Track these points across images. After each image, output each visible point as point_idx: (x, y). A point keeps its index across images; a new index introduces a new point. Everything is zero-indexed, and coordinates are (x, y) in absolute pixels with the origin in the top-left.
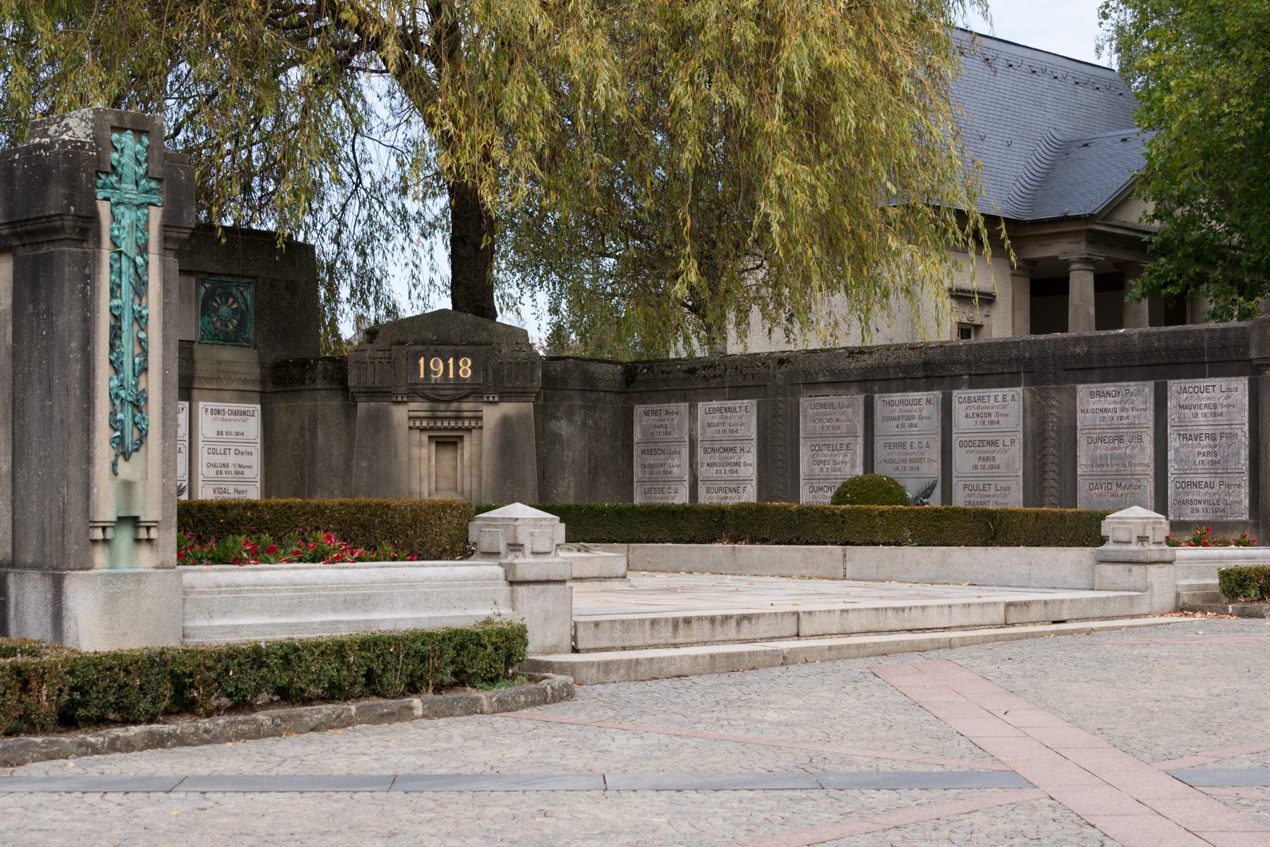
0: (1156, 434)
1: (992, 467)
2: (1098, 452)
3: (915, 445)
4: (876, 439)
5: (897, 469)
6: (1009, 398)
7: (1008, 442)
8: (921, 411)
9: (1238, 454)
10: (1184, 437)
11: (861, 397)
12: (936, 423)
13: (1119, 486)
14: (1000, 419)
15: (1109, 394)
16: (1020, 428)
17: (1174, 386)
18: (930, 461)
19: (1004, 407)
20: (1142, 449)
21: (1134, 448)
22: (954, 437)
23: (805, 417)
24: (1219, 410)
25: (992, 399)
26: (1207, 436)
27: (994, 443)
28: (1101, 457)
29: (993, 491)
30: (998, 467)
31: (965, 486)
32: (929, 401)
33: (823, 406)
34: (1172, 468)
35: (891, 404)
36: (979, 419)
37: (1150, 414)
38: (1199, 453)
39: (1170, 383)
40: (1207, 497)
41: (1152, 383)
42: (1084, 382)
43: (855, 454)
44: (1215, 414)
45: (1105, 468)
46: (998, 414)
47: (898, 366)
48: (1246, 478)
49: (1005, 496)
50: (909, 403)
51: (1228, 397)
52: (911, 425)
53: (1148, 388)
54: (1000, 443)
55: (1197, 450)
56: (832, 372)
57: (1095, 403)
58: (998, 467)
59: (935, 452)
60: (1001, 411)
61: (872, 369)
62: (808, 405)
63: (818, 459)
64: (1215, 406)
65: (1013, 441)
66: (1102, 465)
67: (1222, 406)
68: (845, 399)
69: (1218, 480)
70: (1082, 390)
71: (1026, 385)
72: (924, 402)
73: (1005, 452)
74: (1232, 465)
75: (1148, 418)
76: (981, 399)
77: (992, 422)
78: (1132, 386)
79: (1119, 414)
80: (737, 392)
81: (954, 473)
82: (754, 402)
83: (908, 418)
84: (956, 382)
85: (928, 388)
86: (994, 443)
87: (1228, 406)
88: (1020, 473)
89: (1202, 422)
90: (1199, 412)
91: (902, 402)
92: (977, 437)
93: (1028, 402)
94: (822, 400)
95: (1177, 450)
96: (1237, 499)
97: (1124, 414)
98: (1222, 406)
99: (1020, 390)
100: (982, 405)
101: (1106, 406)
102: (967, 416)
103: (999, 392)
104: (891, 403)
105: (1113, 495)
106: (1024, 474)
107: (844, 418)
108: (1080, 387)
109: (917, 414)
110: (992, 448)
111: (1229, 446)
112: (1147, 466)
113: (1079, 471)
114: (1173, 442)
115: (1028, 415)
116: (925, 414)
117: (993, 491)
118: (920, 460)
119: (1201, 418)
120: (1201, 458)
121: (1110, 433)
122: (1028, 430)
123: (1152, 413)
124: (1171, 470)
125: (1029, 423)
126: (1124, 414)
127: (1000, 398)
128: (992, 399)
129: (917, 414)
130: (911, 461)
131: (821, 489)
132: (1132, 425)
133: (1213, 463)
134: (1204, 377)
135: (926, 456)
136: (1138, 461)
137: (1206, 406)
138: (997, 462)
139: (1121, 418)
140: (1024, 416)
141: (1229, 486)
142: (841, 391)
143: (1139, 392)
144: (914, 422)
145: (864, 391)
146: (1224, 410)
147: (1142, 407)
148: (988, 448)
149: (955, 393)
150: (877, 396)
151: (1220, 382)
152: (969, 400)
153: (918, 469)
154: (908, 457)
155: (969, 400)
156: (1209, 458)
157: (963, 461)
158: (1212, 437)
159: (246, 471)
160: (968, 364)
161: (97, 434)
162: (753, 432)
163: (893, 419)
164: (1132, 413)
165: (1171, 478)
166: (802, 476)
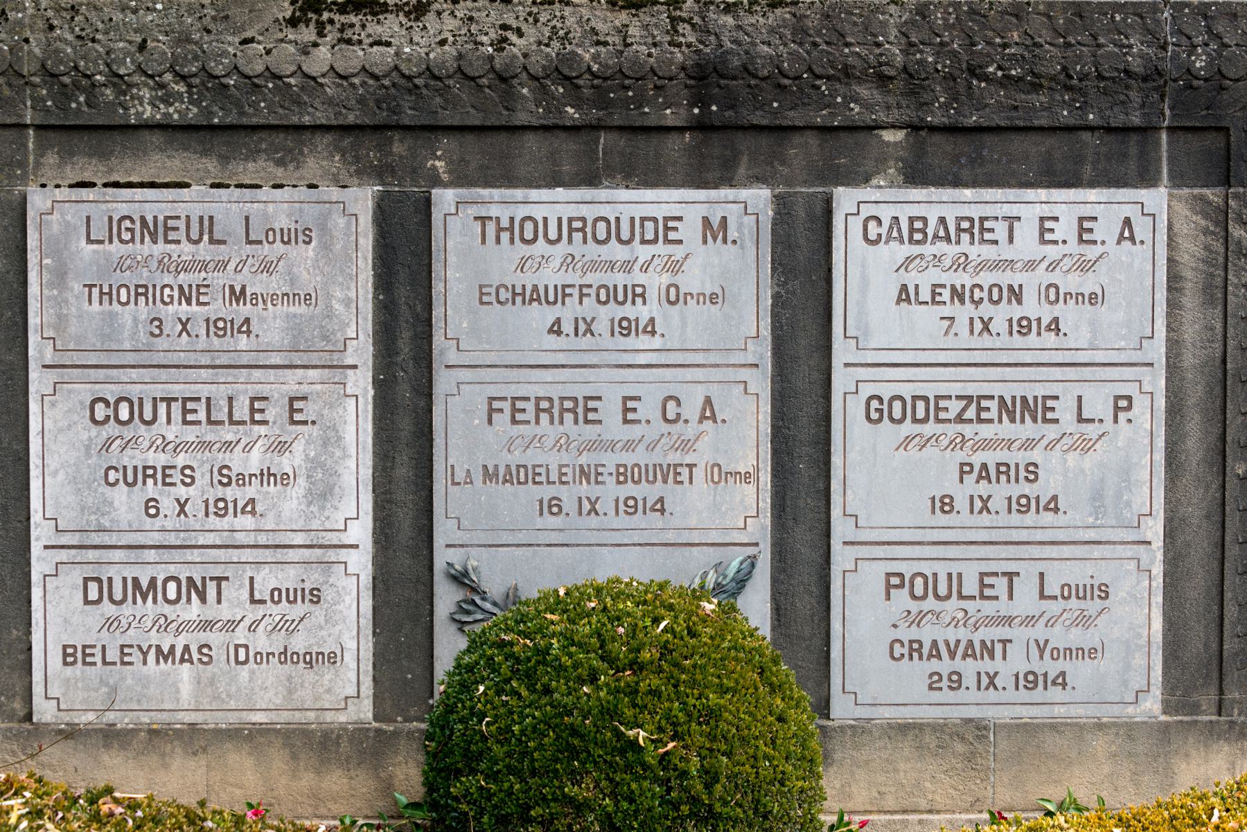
1: (1023, 505)
3: (648, 409)
4: (443, 382)
5: (554, 506)
6: (1106, 230)
7: (1099, 406)
8: (674, 267)
11: (362, 199)
12: (748, 321)
14: (1068, 314)
16: (1158, 351)
18: (721, 475)
19: (1085, 266)
22: (841, 380)
23: (60, 276)
25: (1027, 233)
27: (1036, 409)
29: (1026, 600)
30: (1053, 506)
31: (894, 582)
32: (714, 230)
33: (152, 230)
35: (507, 246)
36: (962, 313)
43: (330, 439)
46: (1052, 294)
47: (563, 73)
49: (1084, 620)
50: (614, 232)
52: (625, 327)
54: (1065, 411)
56: (209, 84)
57: (503, 263)
58: (1053, 506)
59: (745, 433)
60: (1070, 282)
61: (407, 82)
63: (133, 459)
65: (1122, 404)
68: (278, 206)
71: (1178, 180)
72: (689, 230)
73: (1086, 446)
76: (976, 229)
77: (1024, 327)
80: (1114, 155)
81: (840, 529)
82: (760, 197)
83: (610, 296)
84: (845, 151)
85: (705, 173)
86: (1036, 409)
88: (1155, 530)
91: (576, 228)
92: (931, 384)
93: (1191, 251)
94: (154, 204)
99: (1157, 198)
100: (977, 252)
102: (904, 296)
103: (1066, 204)
104: (520, 231)
106: (1170, 534)
107: (274, 284)
109: (656, 281)
110: (1028, 429)
115: (1190, 300)
116: (692, 280)
117: (1026, 600)
118: (669, 473)
122: (1189, 359)
125: (1191, 332)
127: (1065, 229)
128: (1027, 233)
129: (656, 281)
130: (623, 475)
131: (143, 591)
135: (702, 455)
138: (1043, 489)
140: (1173, 306)
142: (250, 170)
144: (642, 312)
145: (380, 173)
148: (1007, 429)
149: (845, 199)
150: (445, 198)
152: (917, 231)
153: (660, 507)
154: (610, 461)
155: (917, 231)
157: (878, 479)
159: (1079, 672)
160: (913, 82)
162: (33, 339)
163: (535, 296)
166: (40, 533)
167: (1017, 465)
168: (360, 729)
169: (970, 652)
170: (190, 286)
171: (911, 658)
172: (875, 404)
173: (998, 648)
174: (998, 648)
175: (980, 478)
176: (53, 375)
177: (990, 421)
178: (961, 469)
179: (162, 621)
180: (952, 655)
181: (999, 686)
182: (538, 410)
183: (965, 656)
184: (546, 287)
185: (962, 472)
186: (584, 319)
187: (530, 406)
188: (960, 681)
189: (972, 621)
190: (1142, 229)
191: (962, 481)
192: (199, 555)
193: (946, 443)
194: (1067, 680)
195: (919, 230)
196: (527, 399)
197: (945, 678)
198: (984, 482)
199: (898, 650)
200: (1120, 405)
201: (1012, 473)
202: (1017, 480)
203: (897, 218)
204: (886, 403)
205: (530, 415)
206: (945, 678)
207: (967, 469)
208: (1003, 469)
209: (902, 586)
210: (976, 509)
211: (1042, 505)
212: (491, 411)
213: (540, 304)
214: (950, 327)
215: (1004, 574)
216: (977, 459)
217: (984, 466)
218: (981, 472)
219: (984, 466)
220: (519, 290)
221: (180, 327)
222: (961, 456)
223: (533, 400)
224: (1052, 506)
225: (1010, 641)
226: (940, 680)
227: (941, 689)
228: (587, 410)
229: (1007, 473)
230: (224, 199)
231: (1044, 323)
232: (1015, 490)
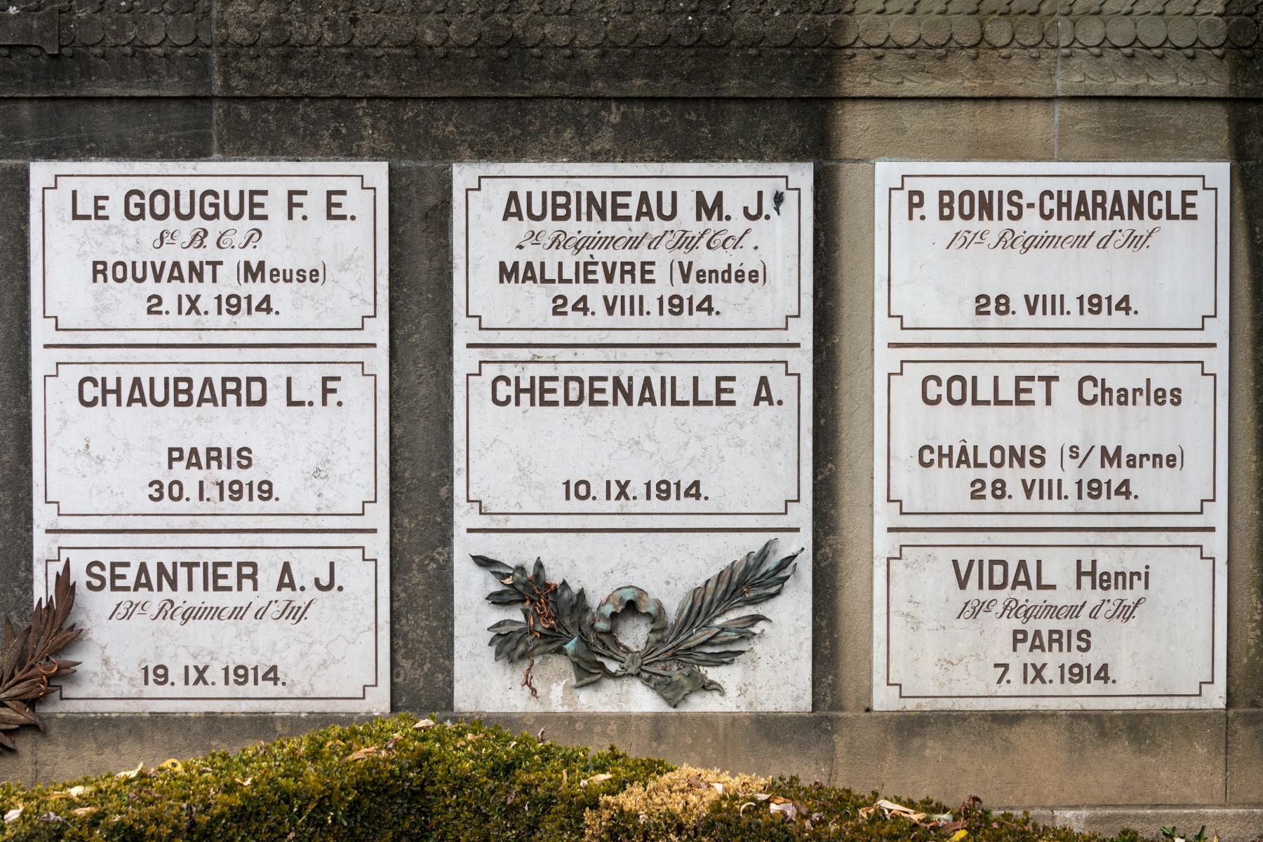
53: (366, 182)
159: (1143, 479)
167: (229, 450)
169: (176, 274)
171: (940, 465)
173: (208, 270)
174: (208, 270)
175: (1033, 648)
176: (478, 354)
178: (1015, 636)
180: (158, 278)
182: (240, 576)
183: (171, 278)
185: (1016, 641)
189: (179, 612)
190: (356, 202)
191: (1015, 650)
195: (183, 392)
199: (927, 457)
201: (224, 459)
202: (1069, 650)
205: (232, 581)
208: (1056, 638)
210: (1030, 678)
211: (1114, 303)
213: (969, 466)
215: (1041, 378)
216: (1031, 626)
217: (1038, 633)
218: (190, 458)
219: (1038, 633)
220: (945, 451)
221: (1044, 673)
222: (1017, 624)
223: (562, 379)
225: (221, 263)
232: (227, 475)
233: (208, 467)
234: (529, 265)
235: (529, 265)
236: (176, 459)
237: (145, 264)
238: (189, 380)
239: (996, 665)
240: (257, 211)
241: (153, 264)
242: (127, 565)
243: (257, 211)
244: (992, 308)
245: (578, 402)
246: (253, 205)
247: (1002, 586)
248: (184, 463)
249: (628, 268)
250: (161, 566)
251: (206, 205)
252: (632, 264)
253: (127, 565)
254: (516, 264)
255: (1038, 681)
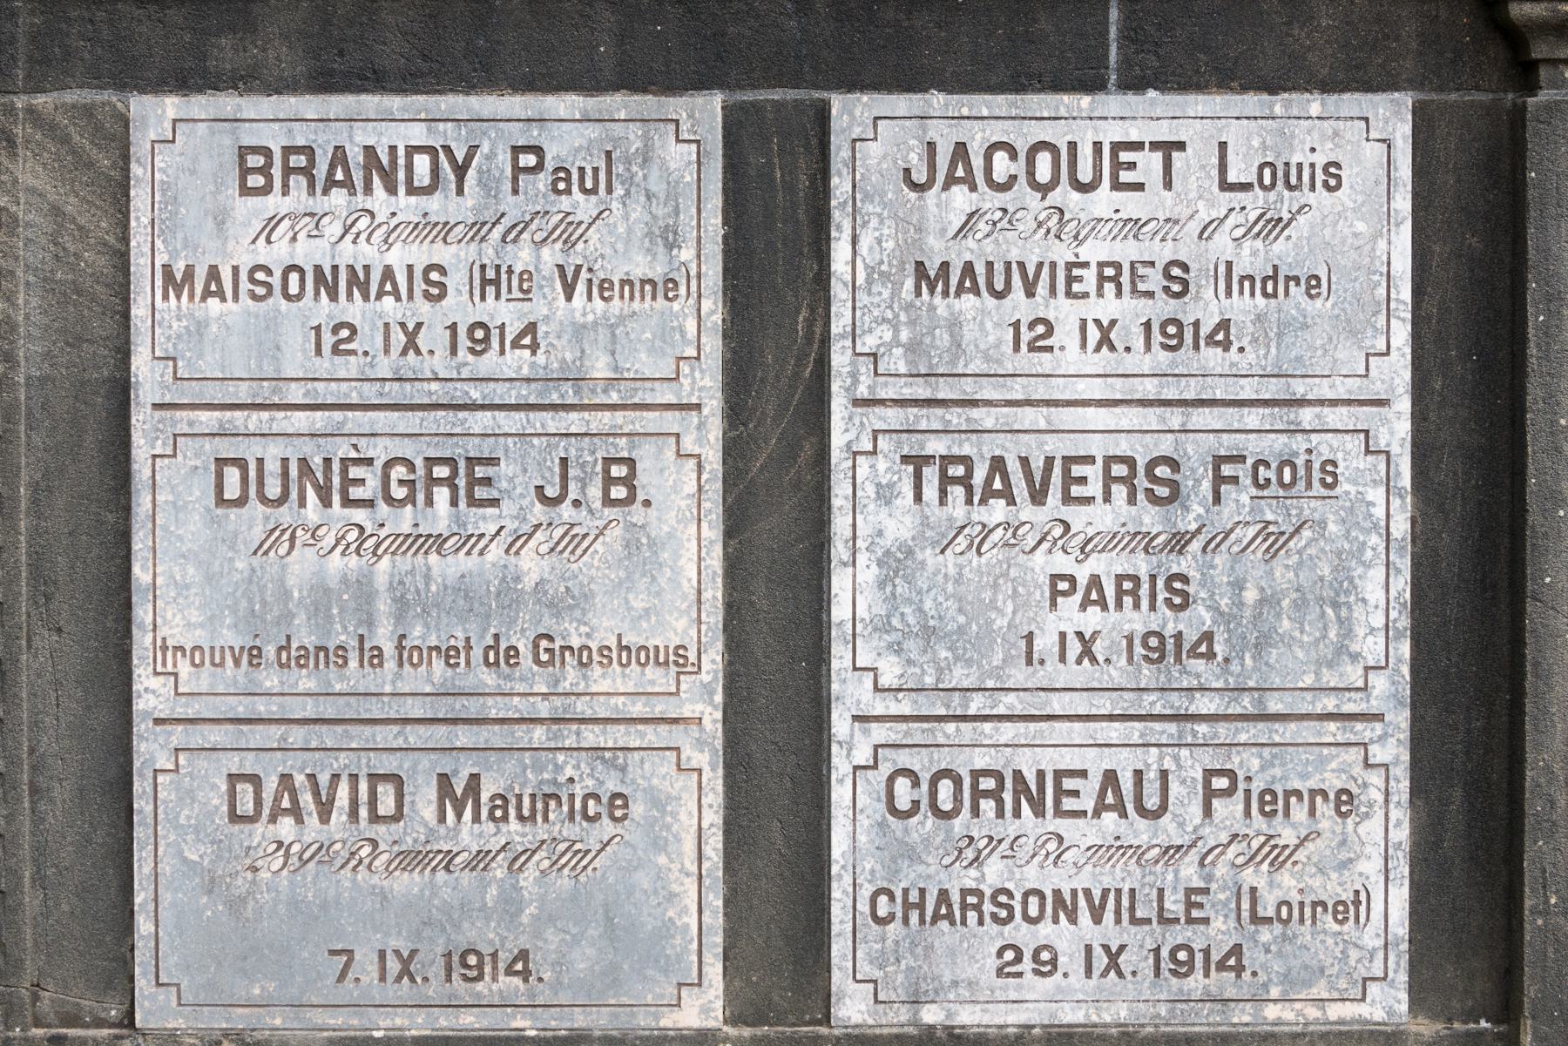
0: (733, 450)
2: (301, 565)
9: (1338, 596)
10: (954, 474)
13: (456, 796)
15: (382, 170)
17: (876, 134)
20: (641, 552)
21: (573, 542)
24: (1206, 308)
26: (1123, 473)
28: (321, 599)
34: (863, 681)
37: (700, 319)
38: (1060, 586)
39: (851, 113)
40: (1119, 875)
41: (705, 112)
42: (185, 81)
44: (1174, 334)
45: (354, 675)
48: (1393, 749)
51: (1275, 225)
53: (679, 143)
55: (1044, 563)
57: (249, 231)
62: (416, 157)
64: (1178, 280)
66: (326, 655)
67: (1229, 279)
69: (1192, 765)
70: (179, 141)
74: (1293, 666)
75: (681, 345)
78: (568, 122)
79: (460, 307)
87: (1272, 282)
89: (1086, 385)
90: (1065, 313)
95: (896, 564)
96: (1333, 888)
97: (505, 313)
98: (1229, 279)
101: (366, 253)
105: (411, 859)
108: (155, 114)
111: (1274, 542)
112: (679, 660)
113: (150, 692)
114: (871, 510)
119: (1070, 355)
120: (1072, 616)
121: (389, 438)
123: (714, 309)
124: (849, 693)
126: (505, 313)
132: (560, 392)
133: (1158, 648)
134: (1093, 84)
136: (605, 629)
137: (1111, 275)
139: (481, 337)
141: (1270, 803)
143: (603, 177)
146: (1243, 307)
147: (640, 266)
151: (1219, 125)
156: (1136, 621)
158: (1159, 481)
161: (1200, 97)
164: (549, 306)
165: (849, 746)
168: (1124, 1033)
170: (990, 265)
172: (399, 472)
177: (1089, 500)
178: (1053, 585)
179: (1052, 846)
181: (1126, 969)
182: (1109, 480)
184: (990, 265)
186: (403, 325)
187: (1093, 472)
188: (1054, 962)
192: (642, 735)
193: (330, 540)
194: (1245, 962)
196: (1090, 460)
197: (1027, 956)
198: (1094, 610)
200: (951, 472)
203: (964, 144)
204: (1022, 157)
206: (1027, 956)
207: (1063, 586)
209: (1229, 792)
212: (1219, 480)
214: (347, 966)
215: (1155, 146)
217: (1095, 581)
219: (1095, 581)
223: (1100, 462)
224: (1203, 649)
226: (1018, 959)
227: (1020, 975)
228: (473, 482)
229: (1134, 593)
230: (1278, 110)
231: (1204, 331)
233: (1119, 605)
234: (968, 268)
235: (968, 268)
236: (1064, 594)
237: (1008, 265)
238: (966, 460)
239: (333, 953)
240: (1125, 176)
241: (1021, 265)
242: (1083, 774)
243: (1125, 176)
244: (1027, 965)
245: (241, 501)
246: (1117, 166)
247: (252, 819)
248: (1078, 597)
249: (1109, 272)
250: (369, 151)
251: (394, 485)
252: (1117, 266)
253: (1083, 774)
254: (945, 266)
255: (1086, 661)
